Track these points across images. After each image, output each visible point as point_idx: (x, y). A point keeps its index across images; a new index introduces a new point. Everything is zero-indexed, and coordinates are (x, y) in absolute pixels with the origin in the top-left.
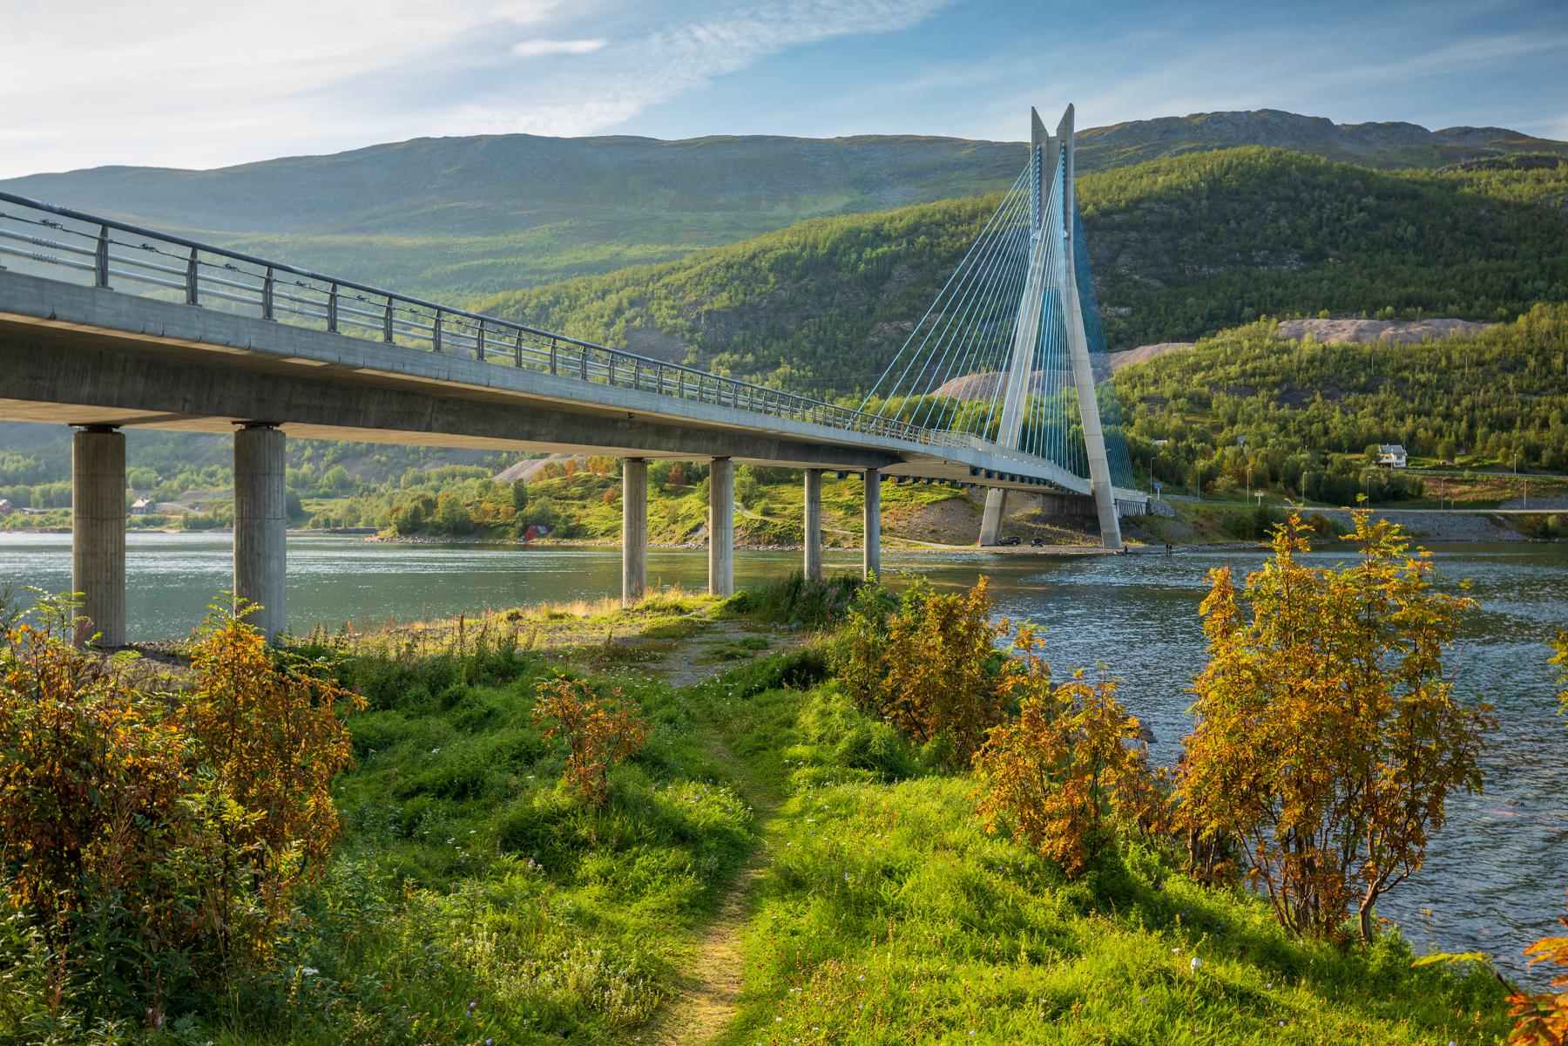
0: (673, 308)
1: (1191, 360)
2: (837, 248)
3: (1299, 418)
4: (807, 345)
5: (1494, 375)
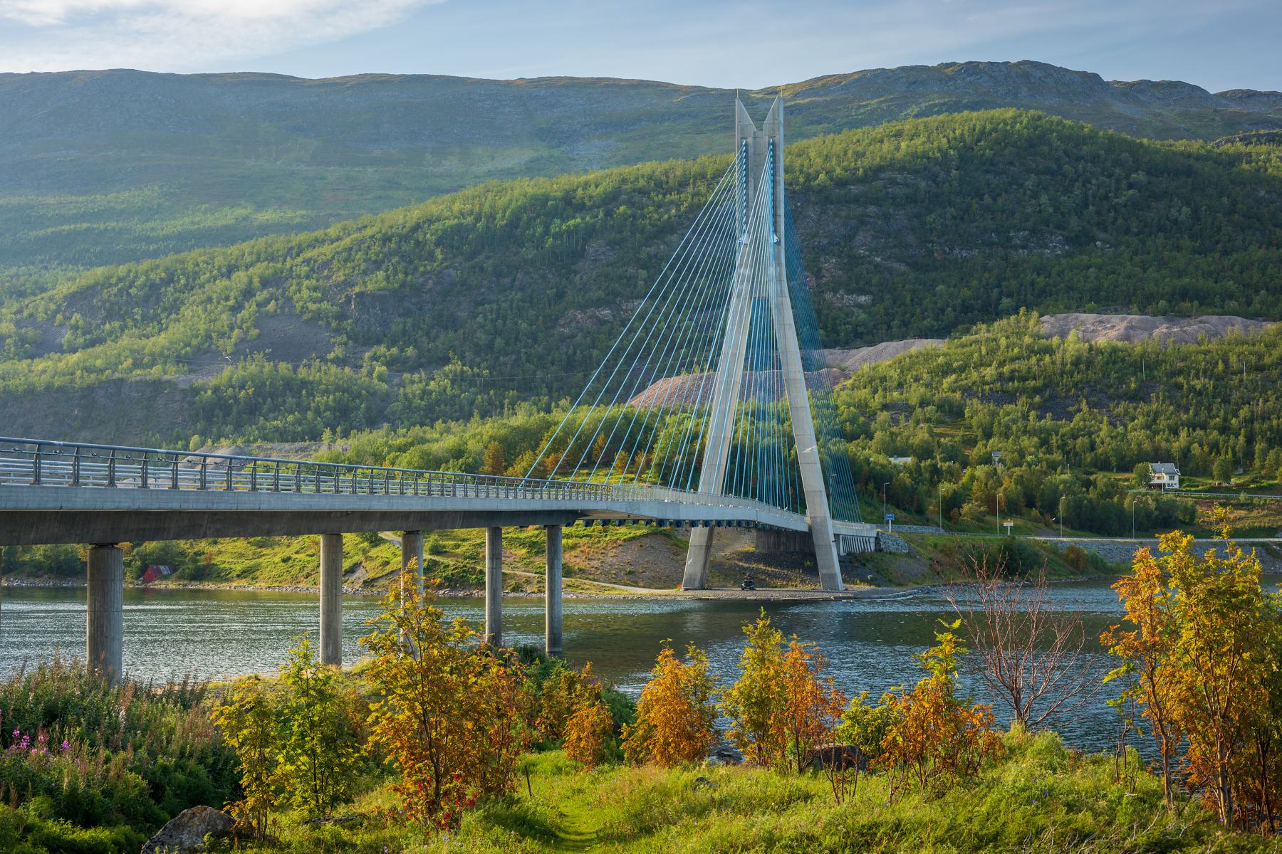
0: (315, 289)
1: (941, 360)
2: (519, 219)
3: (1062, 431)
4: (482, 337)
5: (1275, 382)
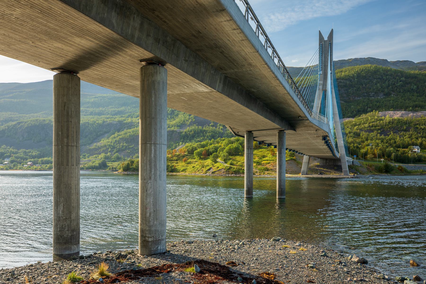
1: (354, 123)
3: (387, 139)
